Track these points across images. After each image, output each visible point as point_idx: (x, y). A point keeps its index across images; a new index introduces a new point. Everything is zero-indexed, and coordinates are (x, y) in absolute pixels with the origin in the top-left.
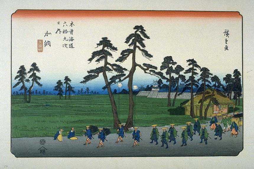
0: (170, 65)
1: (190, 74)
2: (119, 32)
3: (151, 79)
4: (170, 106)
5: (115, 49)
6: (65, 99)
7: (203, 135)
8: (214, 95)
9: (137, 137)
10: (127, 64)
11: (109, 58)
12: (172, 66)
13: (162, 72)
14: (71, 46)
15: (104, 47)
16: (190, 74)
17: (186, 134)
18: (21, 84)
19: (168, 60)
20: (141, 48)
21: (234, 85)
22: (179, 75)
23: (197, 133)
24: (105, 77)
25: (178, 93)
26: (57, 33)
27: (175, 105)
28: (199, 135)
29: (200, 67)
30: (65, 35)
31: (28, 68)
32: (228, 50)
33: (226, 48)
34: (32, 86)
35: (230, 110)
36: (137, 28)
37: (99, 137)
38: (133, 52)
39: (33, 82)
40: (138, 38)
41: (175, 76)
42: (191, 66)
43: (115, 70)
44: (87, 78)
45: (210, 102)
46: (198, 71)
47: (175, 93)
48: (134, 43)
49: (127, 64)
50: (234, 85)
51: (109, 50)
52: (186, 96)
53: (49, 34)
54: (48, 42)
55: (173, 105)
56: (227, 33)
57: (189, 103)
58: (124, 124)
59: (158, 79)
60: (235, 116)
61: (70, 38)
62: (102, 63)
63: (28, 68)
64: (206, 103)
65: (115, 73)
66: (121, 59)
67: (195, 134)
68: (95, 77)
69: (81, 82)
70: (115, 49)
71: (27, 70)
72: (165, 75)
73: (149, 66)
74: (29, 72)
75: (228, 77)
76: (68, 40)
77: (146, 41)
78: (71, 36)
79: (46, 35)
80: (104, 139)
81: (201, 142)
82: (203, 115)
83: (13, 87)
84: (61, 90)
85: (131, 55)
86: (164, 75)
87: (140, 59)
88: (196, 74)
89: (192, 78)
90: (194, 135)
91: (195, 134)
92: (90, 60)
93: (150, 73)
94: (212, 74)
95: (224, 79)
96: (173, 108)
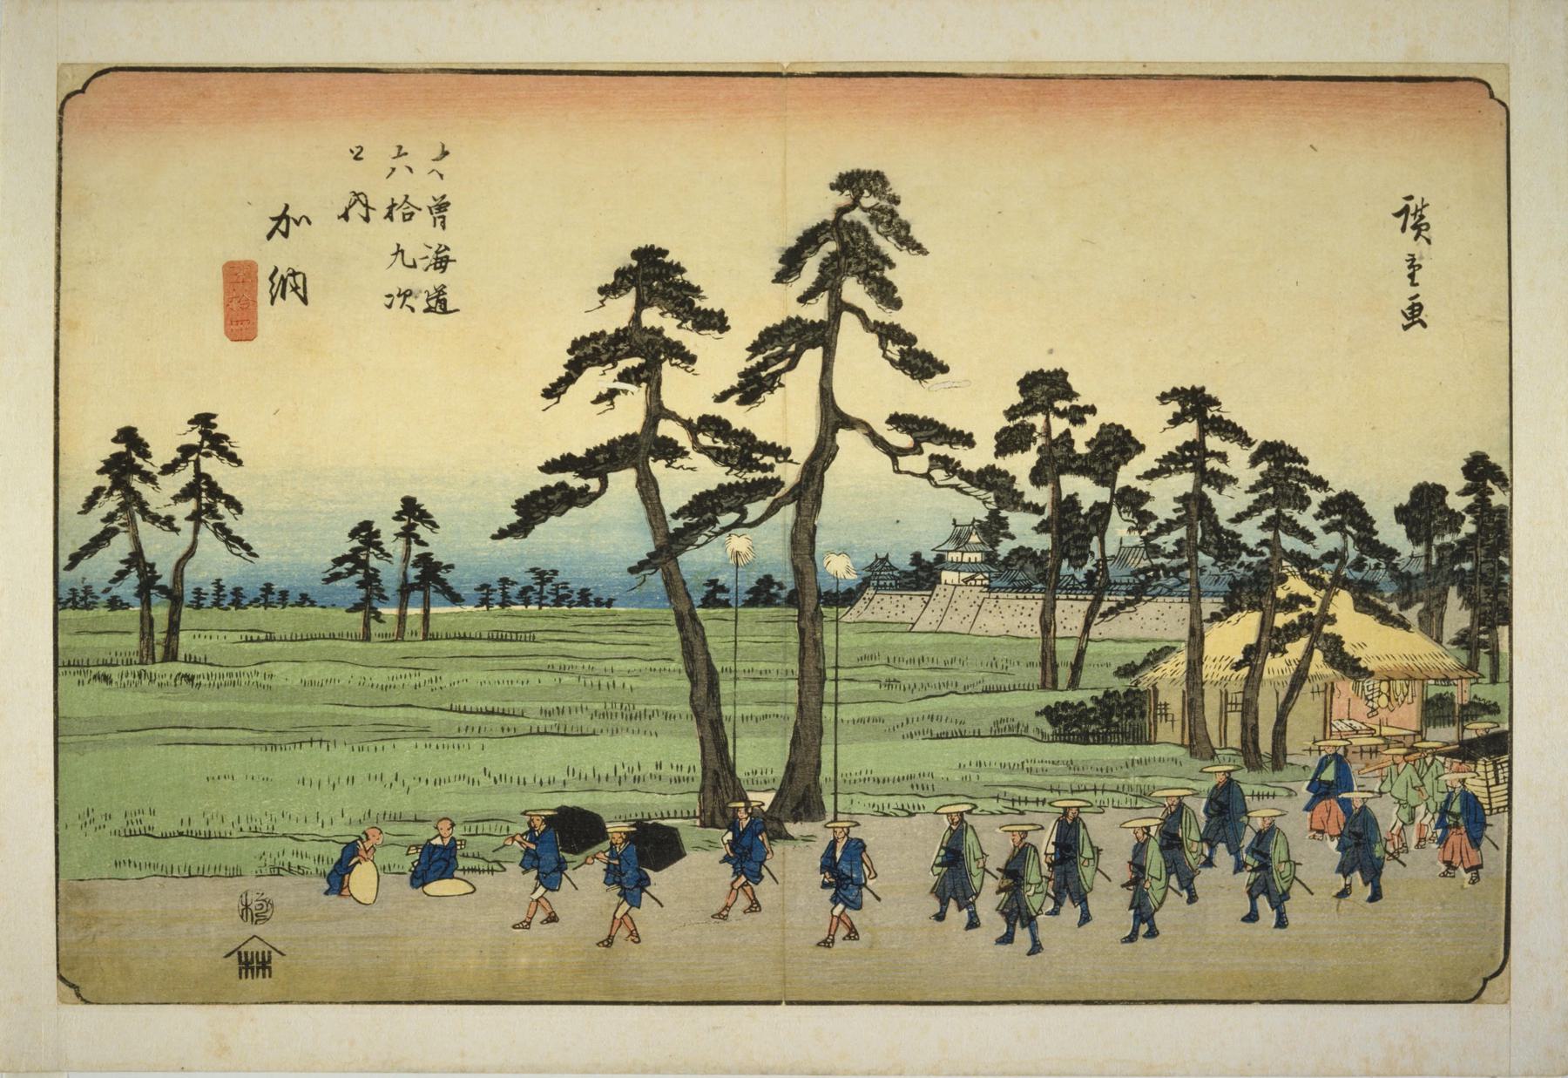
0: (1059, 426)
1: (1184, 482)
2: (735, 235)
3: (928, 513)
4: (1055, 687)
5: (715, 322)
6: (400, 636)
7: (1264, 866)
8: (1332, 620)
9: (800, 494)
10: (785, 418)
11: (670, 373)
12: (1067, 432)
13: (1002, 464)
14: (439, 303)
15: (640, 305)
16: (1184, 482)
17: (1155, 860)
18: (121, 545)
19: (1045, 388)
20: (876, 312)
21: (1459, 548)
22: (1113, 487)
23: (1222, 855)
24: (648, 488)
25: (1105, 606)
26: (345, 216)
27: (1086, 677)
28: (1240, 867)
29: (1246, 441)
30: (398, 231)
31: (165, 437)
32: (1424, 325)
33: (1414, 314)
34: (191, 553)
35: (1436, 710)
36: (851, 182)
37: (613, 875)
38: (822, 336)
39: (196, 531)
40: (850, 246)
41: (1086, 491)
42: (1188, 431)
43: (717, 456)
44: (533, 509)
45: (1309, 652)
46: (1238, 462)
47: (1085, 606)
48: (828, 282)
49: (785, 418)
50: (1459, 548)
51: (671, 327)
52: (1161, 618)
53: (298, 223)
54: (294, 274)
55: (1074, 684)
56: (1413, 218)
57: (1176, 665)
58: (767, 799)
59: (982, 514)
60: (1466, 752)
61: (431, 254)
62: (628, 417)
63: (165, 437)
64: (1277, 667)
65: (711, 475)
66: (752, 387)
67: (1209, 863)
68: (582, 498)
69: (502, 534)
70: (715, 322)
71: (162, 451)
72: (1023, 484)
73: (922, 429)
74: (168, 469)
75: (1423, 508)
76: (415, 266)
77: (904, 271)
78: (437, 237)
79: (276, 227)
80: (643, 890)
81: (1252, 917)
82: (1265, 745)
83: (68, 561)
84: (371, 581)
85: (812, 359)
86: (1018, 487)
87: (867, 379)
88: (1221, 481)
89: (1196, 507)
90: (898, 209)
91: (1209, 863)
92: (553, 392)
93: (927, 476)
94: (1320, 483)
95: (1401, 514)
96: (1073, 697)
